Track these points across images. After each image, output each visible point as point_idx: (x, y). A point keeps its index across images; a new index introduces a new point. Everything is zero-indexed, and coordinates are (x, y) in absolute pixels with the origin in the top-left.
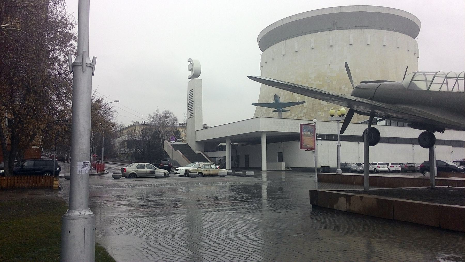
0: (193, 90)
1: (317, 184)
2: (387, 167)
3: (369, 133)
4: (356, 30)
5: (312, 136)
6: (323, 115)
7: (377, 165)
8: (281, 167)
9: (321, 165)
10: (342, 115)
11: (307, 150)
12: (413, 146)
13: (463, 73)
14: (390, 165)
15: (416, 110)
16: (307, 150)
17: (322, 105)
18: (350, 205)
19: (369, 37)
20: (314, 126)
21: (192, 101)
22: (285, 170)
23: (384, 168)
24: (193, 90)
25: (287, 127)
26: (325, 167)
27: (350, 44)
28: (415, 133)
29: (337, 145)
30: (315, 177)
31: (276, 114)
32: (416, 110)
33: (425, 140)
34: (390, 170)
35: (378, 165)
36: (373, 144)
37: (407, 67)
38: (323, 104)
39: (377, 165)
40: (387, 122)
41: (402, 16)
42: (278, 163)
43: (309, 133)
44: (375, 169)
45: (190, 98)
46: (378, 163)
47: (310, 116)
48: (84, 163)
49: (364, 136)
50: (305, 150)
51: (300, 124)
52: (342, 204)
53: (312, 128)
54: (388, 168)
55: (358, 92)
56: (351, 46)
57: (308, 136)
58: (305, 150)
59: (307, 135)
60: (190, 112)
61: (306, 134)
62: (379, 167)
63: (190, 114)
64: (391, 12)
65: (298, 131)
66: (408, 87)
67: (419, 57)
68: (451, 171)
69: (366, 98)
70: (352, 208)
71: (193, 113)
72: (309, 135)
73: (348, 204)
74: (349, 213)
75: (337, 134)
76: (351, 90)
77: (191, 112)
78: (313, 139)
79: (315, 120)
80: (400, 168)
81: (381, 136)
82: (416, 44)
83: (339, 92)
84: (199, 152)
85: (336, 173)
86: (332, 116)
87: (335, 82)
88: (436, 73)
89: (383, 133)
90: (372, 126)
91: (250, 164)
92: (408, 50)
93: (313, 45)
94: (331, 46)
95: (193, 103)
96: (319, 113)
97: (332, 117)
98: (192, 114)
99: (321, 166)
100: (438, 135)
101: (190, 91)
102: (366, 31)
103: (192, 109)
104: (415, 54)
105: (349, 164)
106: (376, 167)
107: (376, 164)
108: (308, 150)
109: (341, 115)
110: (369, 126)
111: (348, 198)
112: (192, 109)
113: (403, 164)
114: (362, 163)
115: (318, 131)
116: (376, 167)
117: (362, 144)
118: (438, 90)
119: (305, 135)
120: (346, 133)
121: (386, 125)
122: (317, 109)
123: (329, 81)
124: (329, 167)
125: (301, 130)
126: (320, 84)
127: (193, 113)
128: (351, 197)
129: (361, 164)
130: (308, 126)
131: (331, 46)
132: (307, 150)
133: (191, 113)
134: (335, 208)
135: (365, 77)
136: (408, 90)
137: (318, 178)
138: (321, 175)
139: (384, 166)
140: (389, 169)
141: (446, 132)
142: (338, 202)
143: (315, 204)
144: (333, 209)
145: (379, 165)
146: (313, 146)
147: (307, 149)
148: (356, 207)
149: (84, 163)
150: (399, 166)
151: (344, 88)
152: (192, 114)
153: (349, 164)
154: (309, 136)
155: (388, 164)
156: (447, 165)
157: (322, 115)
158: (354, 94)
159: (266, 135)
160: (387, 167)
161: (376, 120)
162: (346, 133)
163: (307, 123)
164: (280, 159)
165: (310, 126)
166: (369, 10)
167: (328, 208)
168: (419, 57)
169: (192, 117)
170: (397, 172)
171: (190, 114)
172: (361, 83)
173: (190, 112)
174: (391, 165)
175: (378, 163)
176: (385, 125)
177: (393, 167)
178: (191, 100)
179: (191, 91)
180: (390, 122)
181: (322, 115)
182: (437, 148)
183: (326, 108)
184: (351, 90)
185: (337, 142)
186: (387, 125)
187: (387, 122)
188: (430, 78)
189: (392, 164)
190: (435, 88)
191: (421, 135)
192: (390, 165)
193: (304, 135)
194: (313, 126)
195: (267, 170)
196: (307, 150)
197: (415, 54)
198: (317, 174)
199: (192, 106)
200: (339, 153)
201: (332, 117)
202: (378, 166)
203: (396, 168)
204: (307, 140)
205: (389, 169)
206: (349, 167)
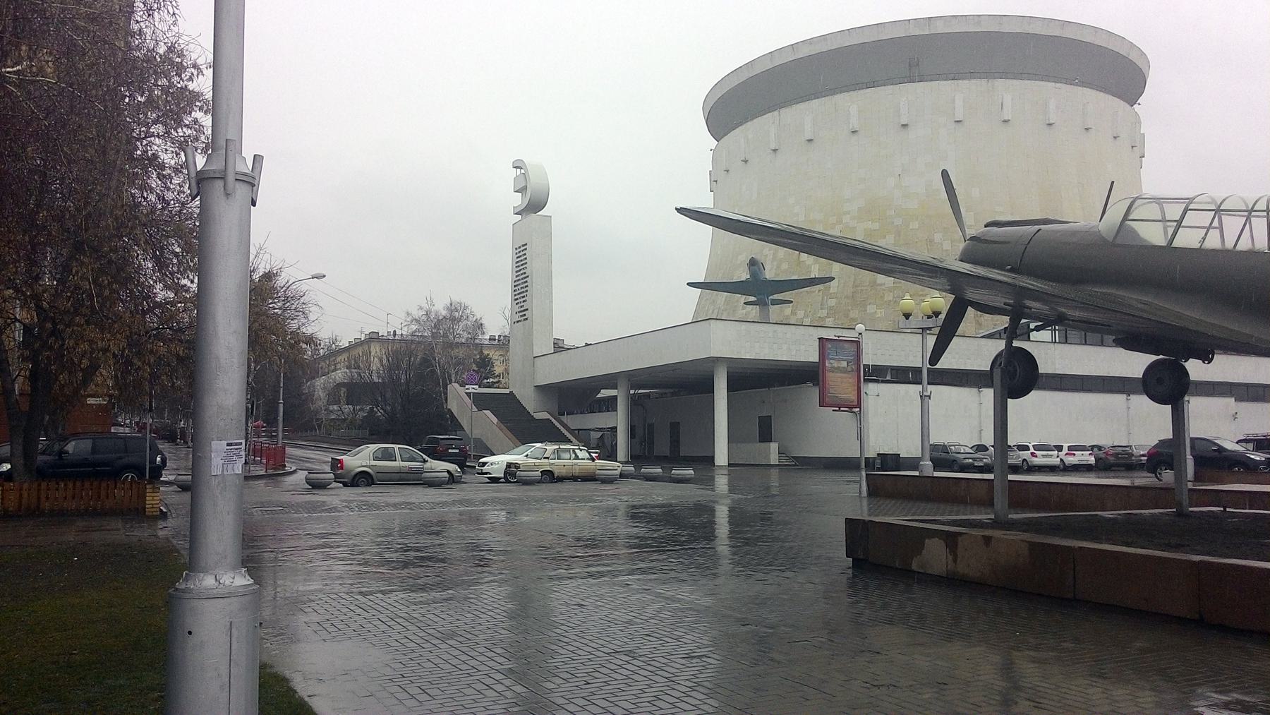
0: (526, 244)
1: (865, 502)
2: (1058, 457)
3: (1009, 362)
4: (973, 81)
5: (853, 371)
6: (881, 313)
7: (1029, 450)
8: (768, 456)
9: (878, 450)
10: (934, 313)
11: (839, 408)
12: (1129, 398)
13: (1266, 198)
14: (1065, 450)
15: (1135, 299)
16: (838, 409)
17: (878, 287)
18: (955, 561)
19: (1008, 100)
20: (857, 344)
21: (525, 276)
22: (778, 463)
23: (1050, 460)
24: (526, 244)
25: (785, 347)
26: (889, 456)
27: (955, 121)
28: (1135, 364)
29: (921, 396)
30: (859, 482)
31: (754, 311)
32: (1135, 299)
33: (1160, 381)
34: (1065, 464)
35: (1032, 450)
36: (1020, 392)
37: (1113, 182)
38: (881, 285)
39: (1029, 450)
40: (1057, 332)
41: (1097, 43)
42: (759, 444)
43: (844, 364)
44: (1024, 460)
45: (519, 266)
46: (1033, 446)
47: (847, 316)
48: (228, 445)
50: (833, 411)
51: (819, 339)
52: (935, 557)
53: (853, 348)
54: (1058, 459)
56: (960, 124)
57: (841, 372)
58: (833, 411)
59: (839, 367)
60: (520, 305)
61: (836, 365)
62: (1036, 457)
63: (519, 312)
64: (1068, 34)
65: (814, 357)
66: (1115, 237)
67: (1144, 157)
68: (1231, 467)
69: (1001, 267)
70: (962, 569)
71: (527, 310)
72: (844, 368)
73: (950, 558)
74: (953, 582)
75: (921, 366)
76: (958, 244)
77: (522, 307)
78: (854, 381)
79: (860, 327)
80: (1093, 459)
81: (1040, 372)
82: (1137, 121)
83: (926, 251)
84: (545, 416)
85: (917, 473)
86: (907, 316)
87: (914, 225)
88: (1191, 200)
89: (1046, 363)
90: (1016, 344)
91: (682, 448)
92: (1115, 138)
93: (855, 123)
94: (903, 125)
95: (527, 282)
96: (871, 309)
97: (907, 319)
98: (524, 310)
99: (878, 454)
100: (1196, 369)
101: (520, 247)
102: (1000, 83)
103: (523, 297)
104: (1132, 147)
105: (953, 448)
106: (1026, 454)
107: (1026, 448)
108: (842, 409)
109: (930, 313)
110: (1009, 344)
111: (951, 540)
112: (523, 297)
113: (1100, 448)
114: (988, 446)
115: (869, 359)
116: (1026, 454)
117: (988, 394)
118: (1197, 246)
119: (834, 370)
120: (945, 363)
121: (1055, 342)
123: (898, 222)
124: (899, 455)
125: (821, 355)
127: (527, 310)
128: (960, 539)
129: (986, 446)
130: (841, 343)
131: (905, 126)
132: (839, 408)
133: (522, 309)
134: (914, 567)
135: (996, 210)
136: (1114, 244)
137: (868, 486)
138: (876, 476)
139: (1050, 453)
140: (1061, 460)
141: (1219, 359)
142: (924, 552)
143: (861, 557)
144: (910, 571)
145: (1035, 450)
146: (854, 397)
147: (839, 406)
148: (973, 564)
149: (228, 445)
150: (1090, 454)
152: (524, 310)
153: (953, 448)
154: (843, 371)
155: (1059, 448)
156: (1221, 449)
157: (880, 313)
158: (966, 257)
159: (727, 368)
160: (1058, 457)
162: (945, 363)
163: (838, 337)
164: (766, 435)
165: (846, 345)
166: (1006, 28)
167: (897, 569)
168: (1144, 157)
169: (525, 320)
170: (1086, 468)
171: (519, 312)
172: (985, 227)
173: (520, 305)
174: (1069, 450)
175: (1033, 446)
176: (1052, 342)
177: (1074, 454)
178: (522, 274)
179: (522, 248)
180: (1066, 332)
181: (880, 313)
182: (1195, 405)
183: (891, 294)
184: (958, 244)
185: (919, 387)
186: (1057, 341)
187: (1057, 332)
188: (1174, 212)
189: (1070, 448)
190: (1187, 239)
191: (1151, 369)
192: (1065, 450)
193: (831, 368)
194: (855, 344)
195: (730, 465)
196: (838, 409)
197: (1132, 147)
198: (866, 474)
199: (524, 290)
200: (927, 416)
201: (907, 319)
202: (1032, 454)
203: (1082, 458)
204: (840, 383)
205: (1061, 460)
206: (954, 454)
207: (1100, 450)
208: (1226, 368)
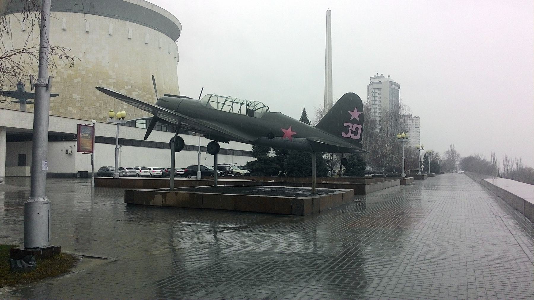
1: (93, 189)
2: (150, 172)
3: (176, 141)
5: (91, 138)
6: (74, 111)
7: (139, 170)
8: (24, 171)
9: (79, 169)
10: (122, 118)
11: (85, 152)
13: (245, 101)
14: (152, 170)
15: (211, 124)
16: (84, 153)
17: (73, 100)
18: (165, 200)
19: (131, 30)
20: (93, 127)
22: (29, 176)
23: (147, 173)
26: (84, 172)
27: (109, 35)
28: (205, 142)
29: (115, 149)
30: (91, 182)
31: (18, 106)
32: (211, 124)
33: (212, 148)
34: (151, 175)
35: (140, 170)
36: (178, 150)
37: (203, 88)
38: (75, 99)
39: (139, 170)
40: (146, 125)
42: (19, 167)
43: (88, 135)
44: (137, 173)
46: (141, 168)
47: (59, 111)
48: (46, 162)
49: (172, 143)
50: (82, 153)
51: (78, 124)
52: (159, 200)
53: (91, 129)
54: (150, 173)
55: (161, 102)
57: (86, 138)
58: (82, 153)
59: (85, 136)
61: (84, 135)
62: (142, 172)
64: (154, 9)
65: (75, 132)
66: (206, 106)
67: (178, 62)
68: (210, 175)
69: (172, 110)
70: (168, 203)
72: (88, 136)
73: (164, 200)
74: (164, 207)
75: (116, 137)
78: (91, 142)
79: (94, 121)
80: (162, 173)
81: (185, 144)
82: (176, 48)
85: (113, 178)
86: (112, 118)
87: (90, 75)
88: (227, 98)
90: (179, 135)
92: (169, 53)
93: (65, 27)
94: (87, 32)
96: (70, 109)
97: (111, 119)
99: (78, 171)
100: (223, 145)
104: (175, 58)
105: (110, 169)
106: (138, 171)
107: (138, 169)
108: (86, 153)
109: (121, 117)
110: (177, 135)
111: (164, 195)
113: (164, 169)
114: (124, 168)
115: (97, 133)
116: (138, 171)
117: (169, 152)
118: (229, 111)
119: (83, 137)
120: (149, 139)
121: (145, 128)
122: (67, 103)
123: (83, 73)
125: (78, 131)
126: (73, 75)
128: (167, 194)
129: (123, 168)
130: (86, 127)
131: (87, 32)
132: (85, 152)
134: (151, 204)
136: (206, 108)
137: (95, 182)
138: (100, 179)
139: (147, 171)
140: (151, 173)
141: (231, 142)
142: (155, 199)
143: (131, 202)
144: (149, 205)
145: (142, 170)
146: (90, 148)
147: (85, 151)
148: (171, 200)
149: (46, 162)
150: (161, 171)
151: (101, 83)
153: (110, 169)
154: (87, 138)
155: (150, 169)
156: (208, 169)
157: (74, 111)
158: (157, 104)
160: (150, 172)
161: (135, 122)
162: (149, 139)
163: (85, 124)
164: (22, 162)
165: (89, 128)
167: (145, 205)
168: (178, 62)
170: (159, 176)
172: (164, 96)
174: (153, 170)
175: (141, 168)
176: (144, 128)
177: (155, 171)
180: (162, 127)
181: (74, 111)
182: (219, 156)
183: (80, 103)
185: (115, 146)
186: (146, 128)
187: (146, 125)
188: (222, 100)
189: (154, 169)
190: (226, 109)
191: (210, 144)
192: (152, 170)
193: (82, 136)
194: (92, 128)
195: (6, 176)
196: (84, 153)
197: (175, 58)
198: (94, 178)
200: (117, 156)
201: (111, 119)
202: (140, 171)
203: (158, 173)
204: (86, 143)
205: (151, 173)
206: (112, 171)
207: (164, 170)
208: (233, 145)
